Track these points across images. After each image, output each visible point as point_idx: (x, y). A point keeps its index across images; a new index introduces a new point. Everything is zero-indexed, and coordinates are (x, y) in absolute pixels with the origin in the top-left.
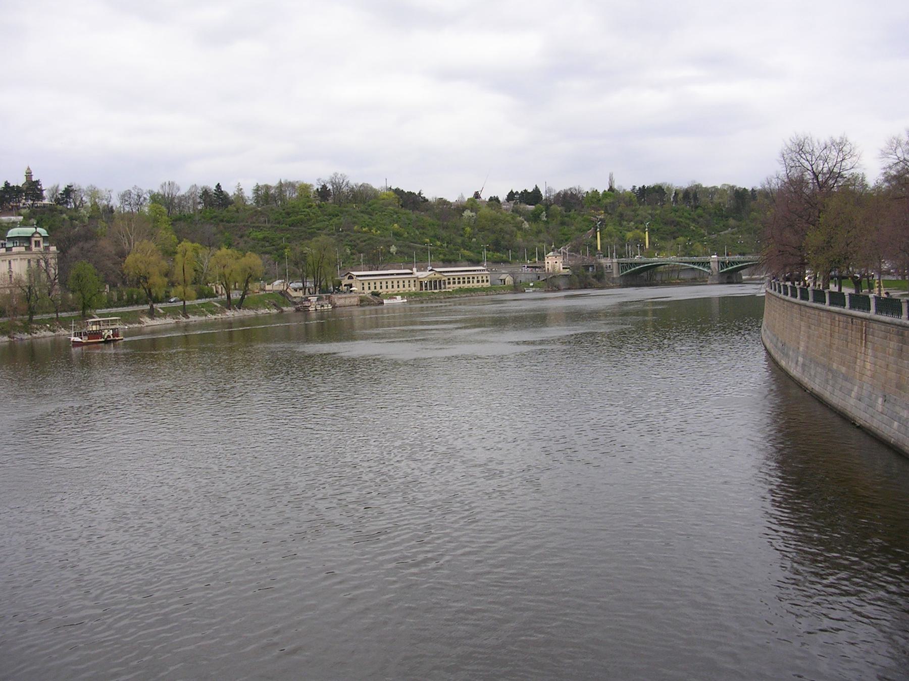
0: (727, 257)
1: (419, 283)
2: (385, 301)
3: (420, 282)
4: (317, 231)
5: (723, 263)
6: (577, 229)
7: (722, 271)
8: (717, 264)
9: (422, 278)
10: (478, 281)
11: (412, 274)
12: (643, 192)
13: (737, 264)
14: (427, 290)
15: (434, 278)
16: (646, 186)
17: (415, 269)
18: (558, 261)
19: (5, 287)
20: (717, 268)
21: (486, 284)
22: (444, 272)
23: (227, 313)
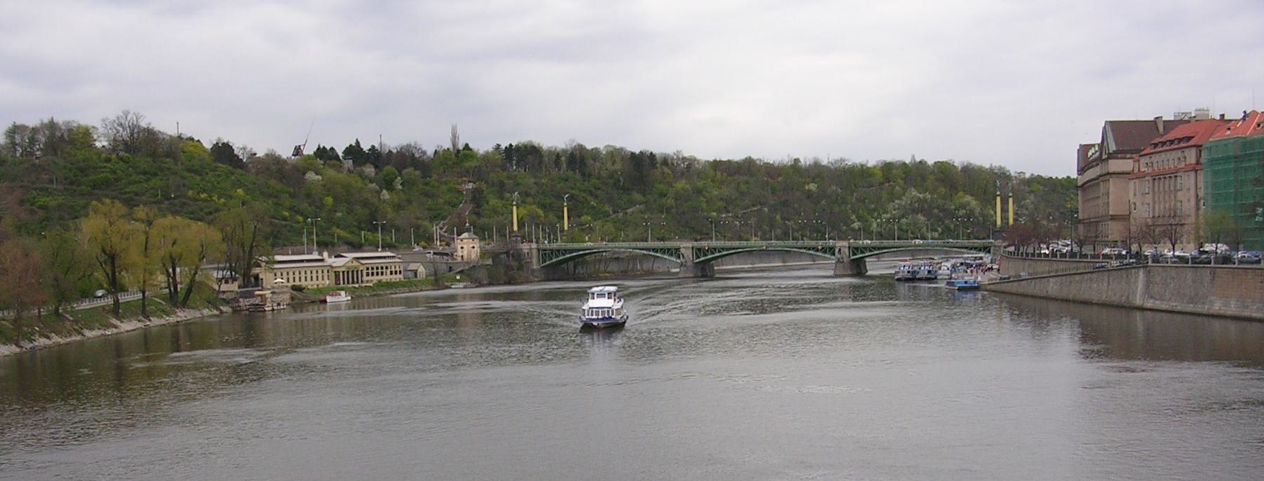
1: (333, 274)
2: (329, 299)
3: (335, 272)
4: (135, 197)
5: (699, 250)
6: (445, 202)
7: (698, 260)
8: (691, 250)
9: (340, 267)
10: (391, 273)
11: (322, 260)
12: (511, 154)
13: (720, 252)
15: (352, 267)
16: (514, 144)
17: (325, 254)
18: (475, 246)
19: (442, 263)
20: (691, 256)
21: (399, 277)
22: (362, 258)
23: (179, 314)
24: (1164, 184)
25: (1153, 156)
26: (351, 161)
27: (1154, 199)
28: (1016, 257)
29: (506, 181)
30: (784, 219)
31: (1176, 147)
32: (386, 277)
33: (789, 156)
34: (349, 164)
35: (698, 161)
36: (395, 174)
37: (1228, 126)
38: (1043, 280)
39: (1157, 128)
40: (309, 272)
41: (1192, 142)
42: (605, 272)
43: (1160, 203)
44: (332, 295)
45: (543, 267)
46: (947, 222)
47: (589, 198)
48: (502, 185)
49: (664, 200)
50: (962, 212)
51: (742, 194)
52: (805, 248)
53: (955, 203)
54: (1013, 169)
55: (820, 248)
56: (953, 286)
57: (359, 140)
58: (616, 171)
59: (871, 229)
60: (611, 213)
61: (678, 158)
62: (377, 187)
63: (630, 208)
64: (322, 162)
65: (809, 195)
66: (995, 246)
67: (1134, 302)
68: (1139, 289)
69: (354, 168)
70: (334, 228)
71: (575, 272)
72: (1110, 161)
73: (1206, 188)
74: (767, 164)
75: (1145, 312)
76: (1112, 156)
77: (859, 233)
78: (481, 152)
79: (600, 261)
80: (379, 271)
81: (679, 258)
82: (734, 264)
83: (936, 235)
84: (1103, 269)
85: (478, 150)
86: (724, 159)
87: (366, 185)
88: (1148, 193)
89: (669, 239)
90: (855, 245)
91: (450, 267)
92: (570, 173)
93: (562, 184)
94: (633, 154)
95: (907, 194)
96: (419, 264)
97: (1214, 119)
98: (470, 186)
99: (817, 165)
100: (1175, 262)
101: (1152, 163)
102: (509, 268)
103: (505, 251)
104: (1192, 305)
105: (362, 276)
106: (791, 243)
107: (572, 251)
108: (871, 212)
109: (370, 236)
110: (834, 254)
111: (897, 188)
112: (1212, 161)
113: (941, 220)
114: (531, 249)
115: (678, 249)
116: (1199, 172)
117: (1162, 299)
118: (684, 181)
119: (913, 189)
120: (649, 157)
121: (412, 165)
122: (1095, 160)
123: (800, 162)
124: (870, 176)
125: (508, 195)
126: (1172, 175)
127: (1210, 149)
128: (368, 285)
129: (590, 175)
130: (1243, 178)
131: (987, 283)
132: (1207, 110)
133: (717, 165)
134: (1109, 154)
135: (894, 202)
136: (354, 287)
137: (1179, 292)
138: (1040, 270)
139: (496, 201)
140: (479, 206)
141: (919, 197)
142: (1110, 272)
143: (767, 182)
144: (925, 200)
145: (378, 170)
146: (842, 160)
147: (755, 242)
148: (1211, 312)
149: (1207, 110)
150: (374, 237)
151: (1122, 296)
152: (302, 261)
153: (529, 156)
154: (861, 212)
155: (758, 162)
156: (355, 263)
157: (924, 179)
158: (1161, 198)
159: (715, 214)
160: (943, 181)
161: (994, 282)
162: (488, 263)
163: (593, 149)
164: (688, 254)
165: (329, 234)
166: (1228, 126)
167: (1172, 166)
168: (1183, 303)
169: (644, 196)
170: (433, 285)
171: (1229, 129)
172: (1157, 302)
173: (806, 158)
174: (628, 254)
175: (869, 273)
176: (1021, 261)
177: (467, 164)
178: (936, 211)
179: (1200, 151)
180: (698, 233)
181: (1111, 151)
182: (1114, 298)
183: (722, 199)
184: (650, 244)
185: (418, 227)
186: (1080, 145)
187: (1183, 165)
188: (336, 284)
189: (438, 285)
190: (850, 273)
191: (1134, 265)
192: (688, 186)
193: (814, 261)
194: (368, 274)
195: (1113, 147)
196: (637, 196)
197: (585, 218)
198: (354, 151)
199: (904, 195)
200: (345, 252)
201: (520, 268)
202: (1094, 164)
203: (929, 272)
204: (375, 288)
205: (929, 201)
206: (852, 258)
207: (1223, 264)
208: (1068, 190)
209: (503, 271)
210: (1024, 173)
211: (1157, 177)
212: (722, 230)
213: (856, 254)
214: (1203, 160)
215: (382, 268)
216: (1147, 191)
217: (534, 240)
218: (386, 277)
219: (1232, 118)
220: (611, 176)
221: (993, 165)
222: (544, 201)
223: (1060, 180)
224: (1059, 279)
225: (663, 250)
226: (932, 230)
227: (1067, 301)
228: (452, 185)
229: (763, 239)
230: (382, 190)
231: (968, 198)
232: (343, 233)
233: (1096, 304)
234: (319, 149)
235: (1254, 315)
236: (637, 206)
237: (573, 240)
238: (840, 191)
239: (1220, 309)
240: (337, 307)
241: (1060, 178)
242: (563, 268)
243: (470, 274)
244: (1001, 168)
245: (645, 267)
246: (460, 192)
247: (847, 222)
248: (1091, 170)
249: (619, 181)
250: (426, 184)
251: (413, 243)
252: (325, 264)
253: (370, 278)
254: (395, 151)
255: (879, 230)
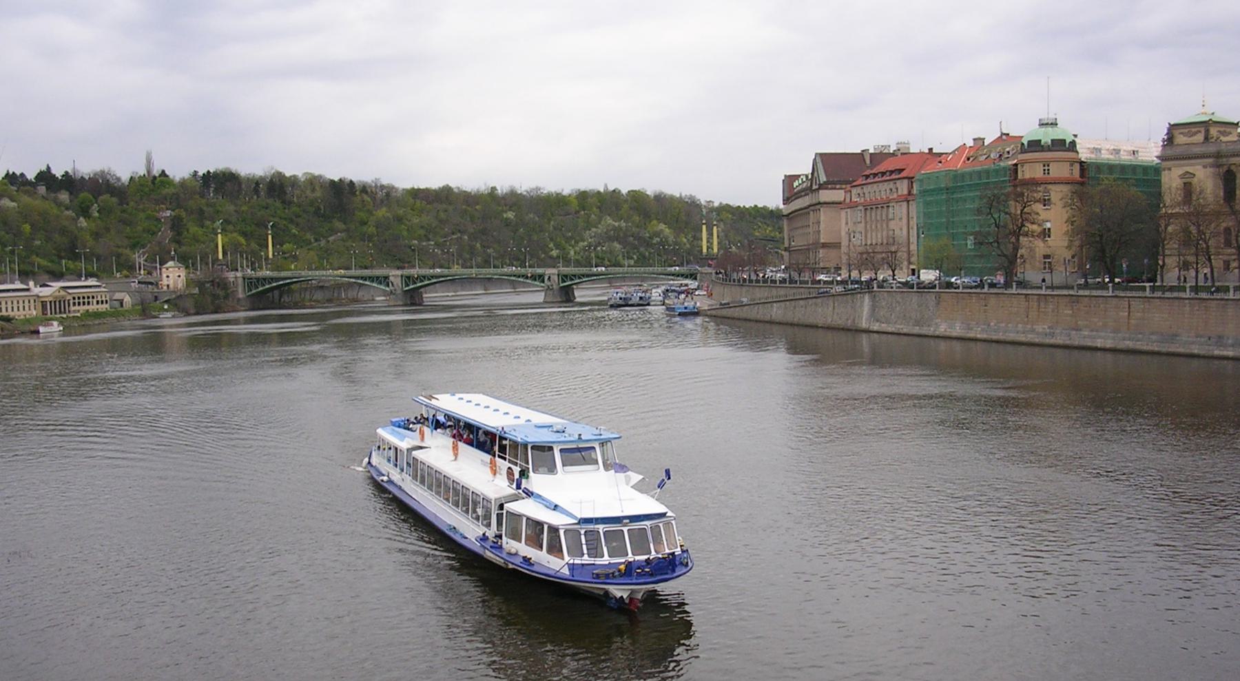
0: (530, 270)
1: (40, 304)
2: (42, 329)
3: (42, 302)
5: (408, 277)
6: (144, 231)
7: (407, 288)
8: (400, 278)
9: (47, 297)
10: (98, 302)
11: (28, 290)
14: (56, 313)
15: (56, 297)
16: (211, 171)
17: (31, 284)
20: (400, 285)
24: (876, 214)
25: (864, 187)
26: (44, 187)
27: (866, 227)
28: (732, 283)
29: (205, 208)
30: (483, 247)
31: (888, 178)
32: (93, 307)
33: (485, 184)
34: (42, 189)
35: (397, 189)
36: (91, 201)
37: (939, 159)
38: (766, 305)
39: (864, 160)
40: (15, 302)
41: (904, 174)
42: (311, 300)
43: (872, 231)
44: (45, 326)
45: (249, 296)
46: (642, 249)
47: (290, 226)
48: (201, 212)
49: (365, 228)
50: (656, 240)
51: (441, 221)
52: (514, 276)
53: (649, 232)
54: (703, 198)
55: (529, 275)
56: (674, 311)
57: (50, 166)
58: (316, 199)
59: (569, 256)
60: (313, 240)
61: (376, 186)
62: (74, 214)
63: (331, 235)
64: (16, 188)
65: (507, 223)
66: (702, 273)
67: (860, 325)
68: (865, 313)
69: (47, 193)
70: (34, 256)
71: (280, 300)
72: (821, 191)
73: (918, 218)
74: (465, 192)
75: (871, 334)
76: (822, 187)
77: (557, 260)
78: (177, 179)
79: (306, 289)
80: (85, 300)
81: (388, 286)
82: (436, 292)
83: (632, 262)
84: (825, 295)
85: (174, 177)
86: (422, 187)
87: (62, 212)
88: (861, 222)
89: (372, 267)
90: (565, 273)
91: (156, 297)
92: (270, 201)
93: (262, 212)
94: (332, 182)
95: (602, 223)
96: (123, 294)
97: (923, 153)
98: (168, 213)
99: (765, 208)
100: (899, 287)
101: (864, 194)
102: (215, 296)
103: (211, 279)
104: (918, 328)
105: (69, 306)
106: (492, 270)
107: (278, 279)
108: (568, 240)
109: (71, 265)
110: (543, 282)
111: (593, 216)
112: (924, 192)
113: (635, 247)
114: (236, 278)
115: (386, 278)
116: (910, 203)
117: (888, 322)
118: (384, 209)
119: (609, 218)
120: (348, 185)
121: (108, 192)
122: (800, 192)
123: (497, 190)
124: (566, 205)
125: (208, 223)
126: (885, 205)
127: (921, 181)
128: (76, 315)
129: (290, 203)
130: (955, 208)
131: (706, 308)
132: (908, 144)
133: (416, 193)
134: (820, 185)
135: (590, 230)
136: (63, 318)
137: (905, 316)
138: (758, 295)
139: (196, 228)
140: (179, 234)
141: (614, 225)
142: (836, 298)
143: (466, 211)
144: (620, 228)
145: (72, 196)
146: (538, 189)
147: (457, 270)
148: (937, 333)
149: (908, 144)
150: (76, 266)
151: (847, 320)
152: (8, 291)
153: (228, 184)
154: (558, 240)
155: (456, 190)
156: (62, 293)
157: (618, 207)
158: (873, 227)
159: (416, 242)
160: (637, 210)
161: (714, 307)
162: (195, 292)
163: (291, 177)
164: (397, 282)
165: (29, 263)
166: (939, 159)
167: (885, 197)
168: (908, 325)
169: (345, 223)
170: (140, 316)
171: (940, 162)
172: (883, 325)
173: (502, 187)
174: (333, 282)
175: (578, 300)
176: (737, 287)
177: (165, 191)
178: (631, 239)
179: (912, 182)
180: (401, 262)
181: (821, 182)
182: (840, 322)
183: (422, 227)
184: (353, 272)
185: (119, 256)
186: (785, 176)
187: (895, 196)
188: (43, 314)
189: (145, 315)
190: (560, 300)
191: (859, 290)
192: (389, 214)
193: (514, 288)
194: (74, 304)
195: (823, 178)
196: (339, 225)
197: (286, 246)
198: (45, 177)
199: (600, 223)
200: (50, 281)
201: (226, 297)
202: (803, 194)
203: (641, 298)
204: (84, 318)
205: (624, 229)
206: (562, 285)
207: (946, 288)
208: (755, 218)
209: (209, 299)
210: (713, 202)
211: (869, 207)
212: (425, 257)
213: (565, 282)
214: (915, 192)
215: (88, 298)
216: (859, 220)
217: (239, 269)
218: (93, 307)
219: (942, 152)
220: (311, 204)
221: (683, 195)
222: (245, 230)
223: (747, 209)
224: (782, 304)
225: (371, 279)
226: (628, 258)
227: (792, 325)
228: (149, 212)
229: (464, 266)
230: (79, 218)
231: (662, 226)
232: (44, 263)
233: (821, 327)
234: (7, 174)
235: (979, 336)
236: (339, 234)
237: (279, 269)
238: (537, 219)
239: (945, 331)
240: (51, 335)
241: (747, 207)
242: (269, 297)
243: (177, 303)
244: (691, 197)
245: (350, 296)
246: (158, 220)
247: (545, 248)
248: (800, 200)
249: (319, 209)
250: (124, 211)
251: (115, 272)
252: (32, 294)
253: (77, 308)
254: (87, 178)
255: (577, 257)
